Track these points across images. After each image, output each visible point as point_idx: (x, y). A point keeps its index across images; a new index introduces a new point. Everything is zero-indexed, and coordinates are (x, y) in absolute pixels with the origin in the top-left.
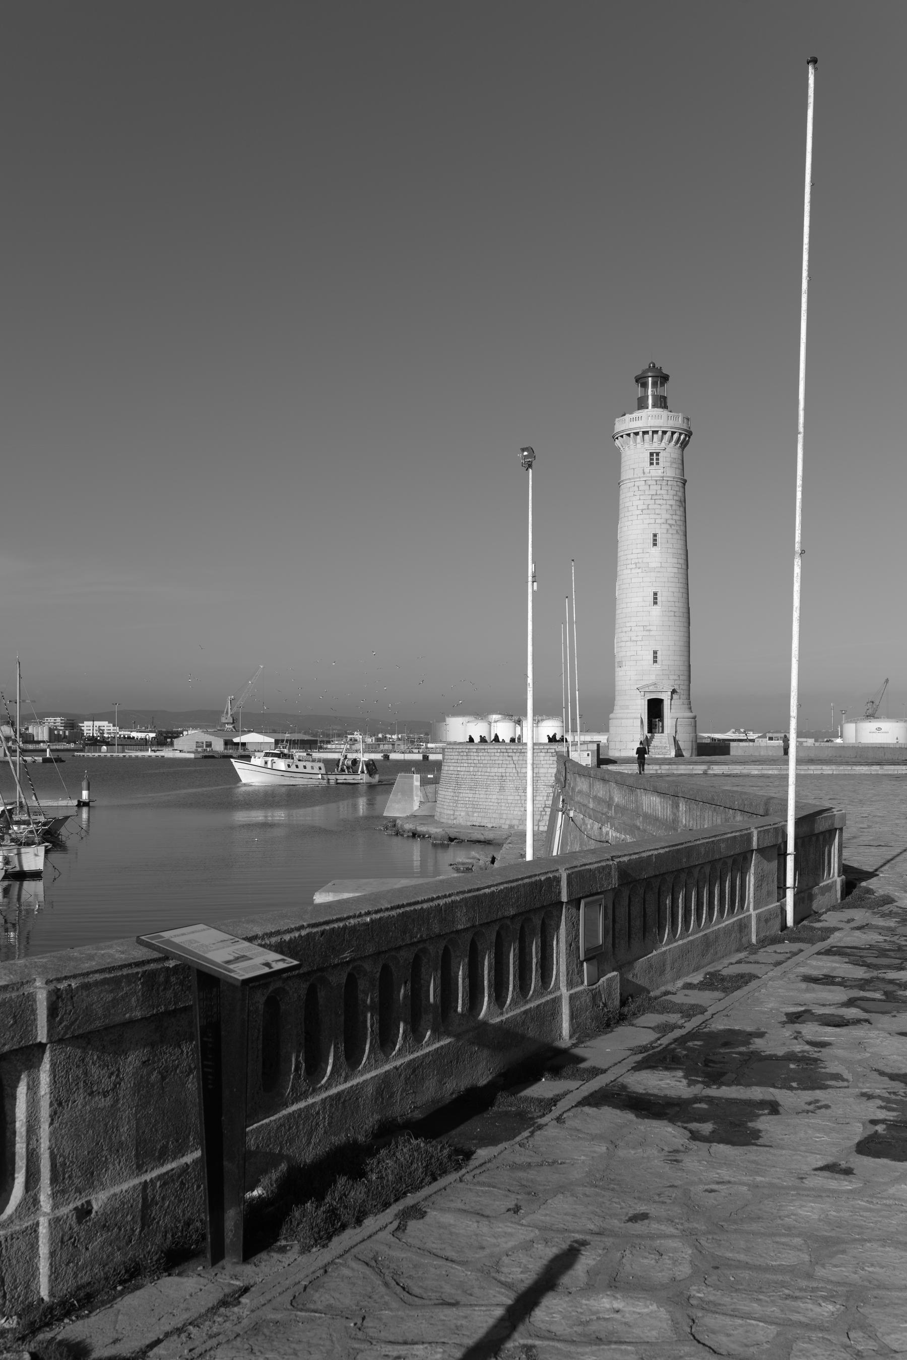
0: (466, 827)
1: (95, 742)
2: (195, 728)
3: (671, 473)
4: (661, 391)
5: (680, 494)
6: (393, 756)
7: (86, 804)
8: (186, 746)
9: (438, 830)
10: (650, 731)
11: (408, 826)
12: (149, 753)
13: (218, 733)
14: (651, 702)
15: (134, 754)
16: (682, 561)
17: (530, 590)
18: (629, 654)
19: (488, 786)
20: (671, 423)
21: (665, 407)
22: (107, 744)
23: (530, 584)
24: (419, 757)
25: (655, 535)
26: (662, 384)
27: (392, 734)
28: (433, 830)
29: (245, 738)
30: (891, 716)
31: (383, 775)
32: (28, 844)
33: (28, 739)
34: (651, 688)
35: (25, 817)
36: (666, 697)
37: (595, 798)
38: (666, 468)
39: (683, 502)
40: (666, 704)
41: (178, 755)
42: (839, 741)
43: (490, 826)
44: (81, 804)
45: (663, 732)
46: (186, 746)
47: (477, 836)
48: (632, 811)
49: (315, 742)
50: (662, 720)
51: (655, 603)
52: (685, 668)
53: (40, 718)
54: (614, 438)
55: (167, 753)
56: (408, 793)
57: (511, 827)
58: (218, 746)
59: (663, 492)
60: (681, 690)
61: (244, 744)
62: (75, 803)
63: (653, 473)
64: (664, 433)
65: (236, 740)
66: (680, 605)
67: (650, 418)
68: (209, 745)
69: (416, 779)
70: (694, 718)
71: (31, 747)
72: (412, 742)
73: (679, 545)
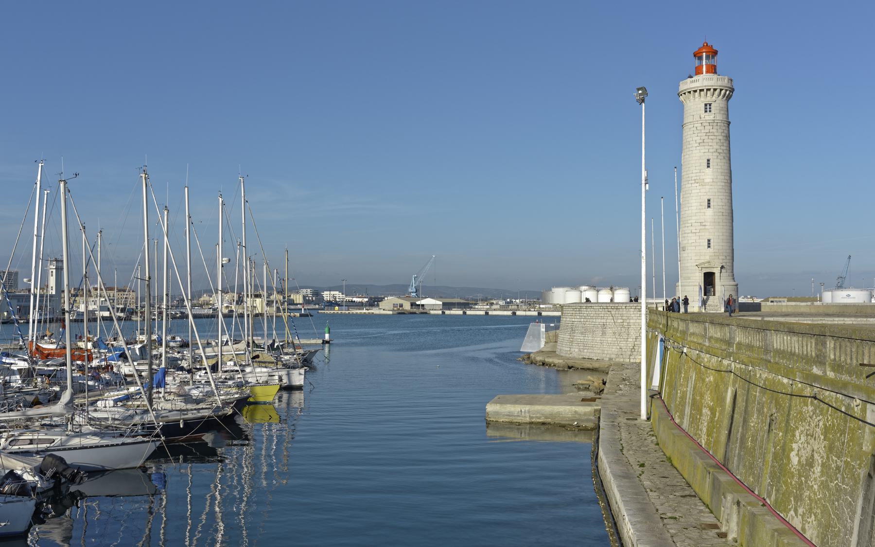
0: (579, 359)
1: (331, 304)
2: (392, 295)
3: (720, 117)
4: (712, 62)
5: (726, 132)
6: (518, 313)
7: (328, 342)
8: (387, 307)
9: (561, 361)
10: (705, 295)
11: (539, 358)
12: (364, 311)
13: (408, 298)
14: (705, 274)
15: (355, 311)
16: (728, 178)
17: (643, 190)
18: (690, 242)
19: (594, 332)
20: (720, 83)
21: (715, 72)
22: (339, 305)
23: (643, 185)
24: (536, 313)
25: (708, 160)
26: (713, 57)
27: (516, 299)
28: (556, 361)
29: (423, 302)
30: (857, 287)
31: (518, 327)
32: (294, 368)
33: (291, 302)
34: (706, 265)
35: (291, 350)
36: (717, 271)
37: (710, 338)
38: (716, 114)
39: (728, 137)
40: (717, 276)
41: (382, 312)
42: (818, 303)
43: (595, 358)
44: (325, 342)
45: (714, 295)
46: (387, 307)
47: (587, 365)
48: (759, 348)
49: (468, 304)
50: (714, 287)
51: (709, 207)
52: (730, 251)
53: (296, 290)
54: (679, 95)
55: (375, 311)
56: (538, 337)
57: (610, 359)
58: (407, 306)
59: (714, 130)
60: (728, 266)
61: (423, 305)
62: (320, 341)
63: (707, 118)
64: (715, 90)
65: (418, 303)
66: (726, 207)
67: (704, 80)
68: (401, 306)
69: (543, 327)
70: (737, 285)
71: (292, 307)
72: (530, 305)
73: (726, 167)
